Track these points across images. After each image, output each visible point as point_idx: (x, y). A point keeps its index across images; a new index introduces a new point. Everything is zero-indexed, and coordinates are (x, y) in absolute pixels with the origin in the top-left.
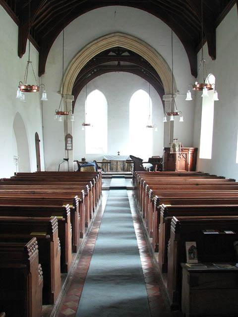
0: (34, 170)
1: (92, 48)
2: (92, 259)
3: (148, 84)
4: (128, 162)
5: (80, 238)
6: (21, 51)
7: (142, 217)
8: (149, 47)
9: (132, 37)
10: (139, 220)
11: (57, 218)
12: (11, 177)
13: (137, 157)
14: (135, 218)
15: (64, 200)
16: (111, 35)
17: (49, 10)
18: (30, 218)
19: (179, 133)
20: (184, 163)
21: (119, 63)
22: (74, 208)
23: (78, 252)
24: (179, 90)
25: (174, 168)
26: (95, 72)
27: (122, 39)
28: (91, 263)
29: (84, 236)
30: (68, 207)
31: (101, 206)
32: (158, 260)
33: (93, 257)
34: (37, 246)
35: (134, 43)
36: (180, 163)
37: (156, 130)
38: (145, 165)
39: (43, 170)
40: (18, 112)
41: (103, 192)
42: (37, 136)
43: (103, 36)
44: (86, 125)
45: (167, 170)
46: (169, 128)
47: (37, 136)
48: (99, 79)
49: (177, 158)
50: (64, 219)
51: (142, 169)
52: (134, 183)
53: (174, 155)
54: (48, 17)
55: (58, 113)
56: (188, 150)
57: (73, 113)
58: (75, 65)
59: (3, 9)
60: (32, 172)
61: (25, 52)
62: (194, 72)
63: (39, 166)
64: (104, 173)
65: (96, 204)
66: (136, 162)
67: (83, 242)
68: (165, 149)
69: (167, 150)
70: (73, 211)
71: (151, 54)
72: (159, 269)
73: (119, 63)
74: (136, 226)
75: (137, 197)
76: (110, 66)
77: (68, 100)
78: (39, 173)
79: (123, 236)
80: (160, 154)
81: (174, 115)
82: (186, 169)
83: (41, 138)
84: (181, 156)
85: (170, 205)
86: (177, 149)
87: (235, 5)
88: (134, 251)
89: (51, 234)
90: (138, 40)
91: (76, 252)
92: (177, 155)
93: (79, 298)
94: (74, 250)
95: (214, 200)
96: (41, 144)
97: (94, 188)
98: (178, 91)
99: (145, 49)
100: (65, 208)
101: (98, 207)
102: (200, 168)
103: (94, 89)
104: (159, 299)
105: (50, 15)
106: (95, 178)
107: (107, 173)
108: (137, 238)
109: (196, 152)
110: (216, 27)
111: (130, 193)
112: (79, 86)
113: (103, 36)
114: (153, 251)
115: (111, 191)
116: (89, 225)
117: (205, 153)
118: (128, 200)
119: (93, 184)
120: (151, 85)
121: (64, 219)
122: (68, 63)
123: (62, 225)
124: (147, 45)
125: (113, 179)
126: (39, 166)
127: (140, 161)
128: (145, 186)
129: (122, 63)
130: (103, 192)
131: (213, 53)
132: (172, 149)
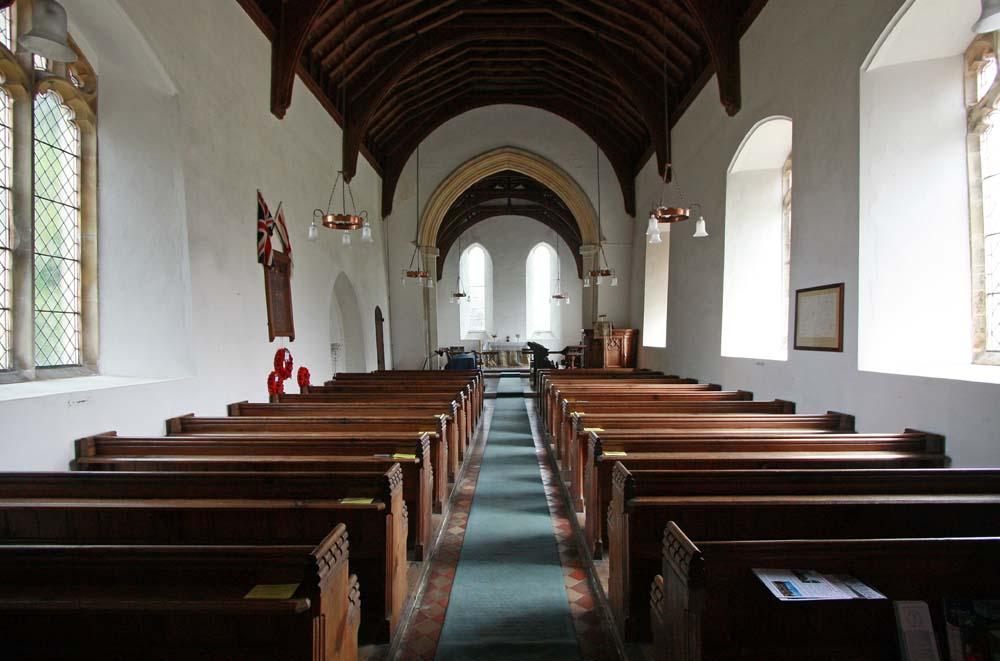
0: (372, 367)
1: (468, 172)
2: (458, 572)
3: (555, 234)
4: (525, 352)
5: (434, 512)
6: (280, 101)
7: (555, 456)
8: (559, 171)
9: (528, 154)
10: (549, 461)
11: (430, 436)
12: (326, 384)
13: (786, 270)
14: (542, 456)
15: (396, 446)
16: (495, 152)
17: (396, 109)
18: (300, 503)
19: (607, 306)
20: (616, 354)
21: (509, 200)
22: (438, 435)
23: (427, 558)
24: (607, 237)
25: (601, 364)
26: (473, 217)
27: (513, 158)
28: (453, 597)
29: (446, 508)
30: (424, 435)
31: (481, 429)
32: (606, 589)
33: (461, 571)
34: (401, 476)
35: (533, 164)
36: (610, 355)
37: (568, 301)
38: (551, 357)
39: (388, 367)
40: (343, 273)
41: (487, 403)
42: (378, 312)
43: (484, 153)
44: (461, 295)
45: (589, 365)
46: (590, 299)
47: (378, 312)
48: (479, 227)
49: (606, 346)
50: (417, 461)
51: (549, 365)
52: (533, 387)
53: (600, 343)
54: (396, 120)
55: (410, 274)
56: (624, 333)
57: (439, 277)
58: (441, 198)
59: (315, 99)
60: (369, 371)
61: (355, 173)
62: (630, 208)
63: (381, 360)
64: (488, 369)
65: (472, 428)
66: (539, 351)
67: (442, 526)
68: (586, 332)
69: (588, 333)
70: (434, 443)
71: (560, 181)
72: (612, 624)
73: (509, 200)
74: (545, 475)
75: (541, 411)
76: (495, 207)
77: (430, 255)
78: (381, 373)
79: (524, 505)
80: (577, 338)
81: (602, 275)
82: (620, 362)
83: (385, 315)
84: (613, 344)
85: (623, 454)
86: (605, 332)
87: (715, 76)
88: (530, 443)
89: (387, 499)
90: (540, 159)
91: (421, 560)
92: (606, 342)
93: (439, 627)
94: (415, 551)
95: (743, 443)
96: (386, 325)
97: (469, 403)
98: (605, 239)
99: (549, 172)
100: (440, 420)
101: (476, 432)
102: (644, 363)
103: (472, 242)
104: (593, 617)
105: (399, 117)
106: (471, 384)
107: (492, 369)
108: (536, 444)
109: (637, 336)
110: (636, 174)
111: (529, 404)
112: (449, 237)
113: (484, 153)
114: (590, 556)
115: (500, 401)
116: (456, 478)
117: (655, 335)
118: (526, 417)
119: (466, 393)
120: (561, 238)
121: (417, 461)
122: (425, 202)
123: (412, 472)
124: (553, 166)
125: (501, 379)
126: (381, 360)
127: (545, 352)
128: (560, 400)
129: (514, 201)
130: (487, 403)
131: (665, 173)
132: (596, 331)
